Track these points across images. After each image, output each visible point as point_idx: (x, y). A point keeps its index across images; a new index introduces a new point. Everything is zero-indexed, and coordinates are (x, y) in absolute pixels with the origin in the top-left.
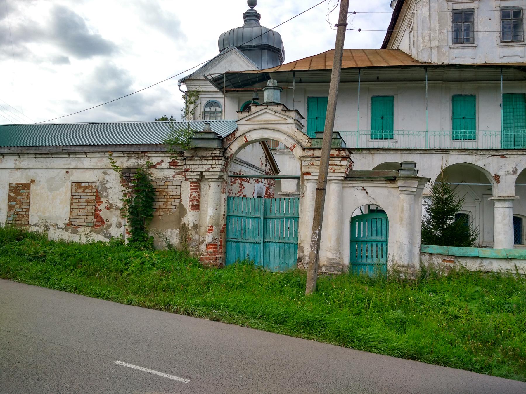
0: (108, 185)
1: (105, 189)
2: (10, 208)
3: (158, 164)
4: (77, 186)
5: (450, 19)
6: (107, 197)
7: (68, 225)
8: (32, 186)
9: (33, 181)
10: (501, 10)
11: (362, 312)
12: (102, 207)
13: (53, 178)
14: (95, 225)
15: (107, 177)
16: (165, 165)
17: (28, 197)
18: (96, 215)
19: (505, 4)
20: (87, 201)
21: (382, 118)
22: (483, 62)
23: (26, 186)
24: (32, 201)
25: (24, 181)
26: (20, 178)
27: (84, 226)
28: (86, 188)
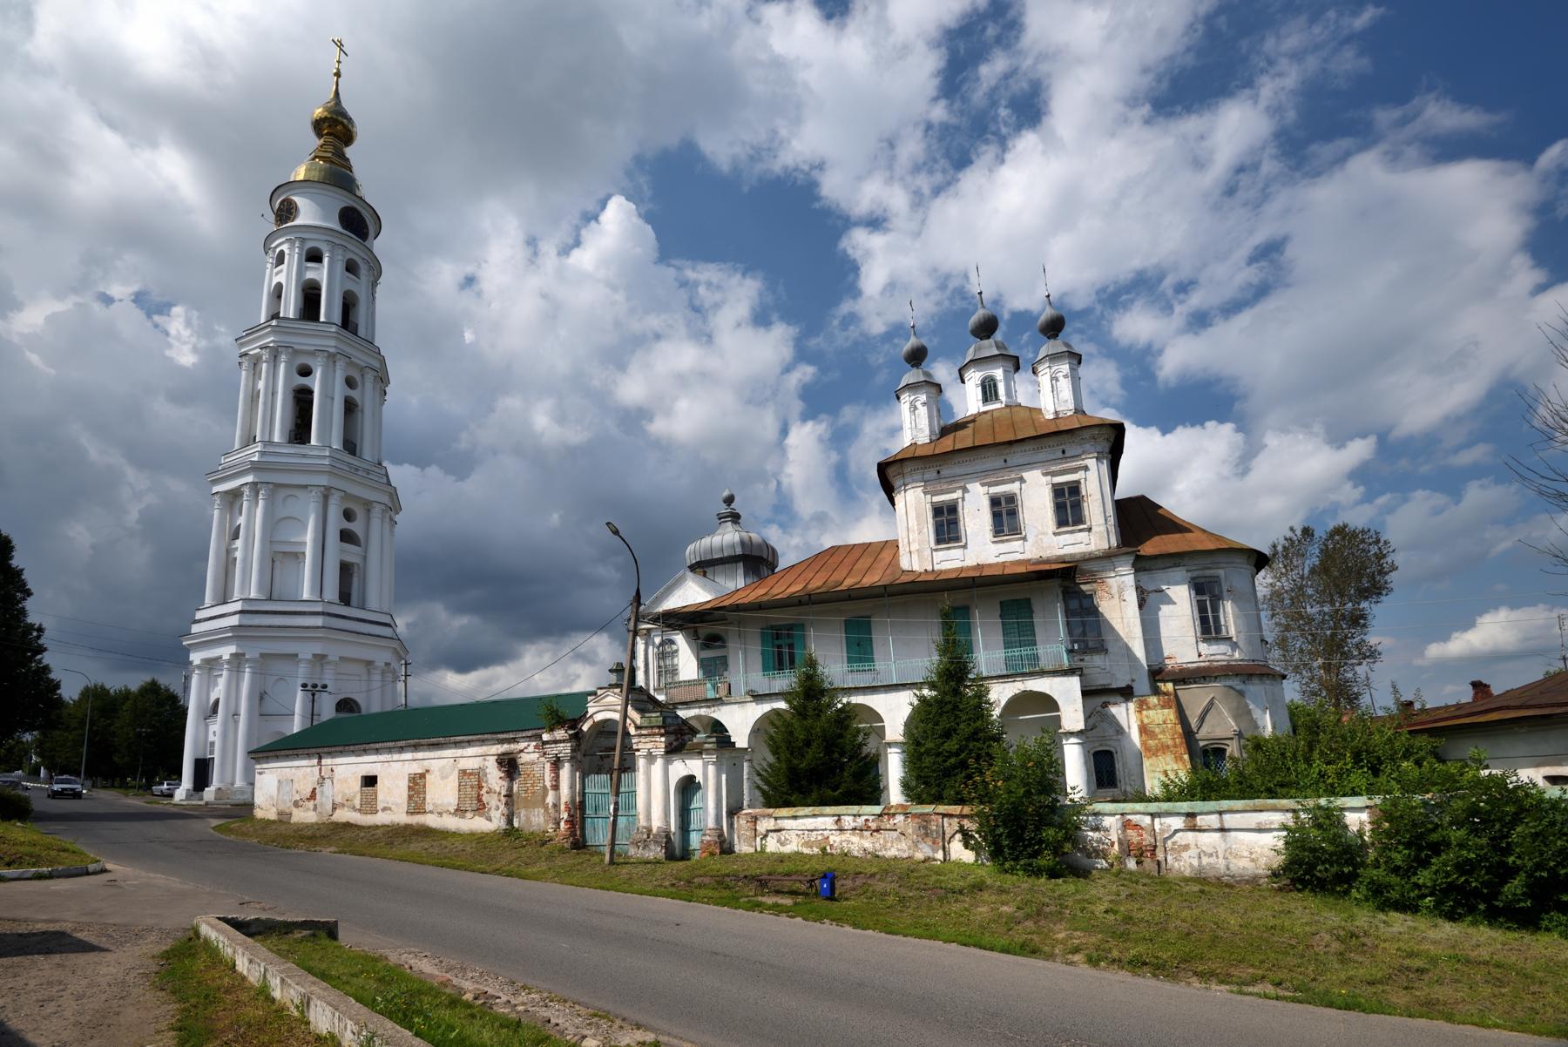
0: (488, 771)
1: (486, 775)
2: (410, 797)
3: (526, 748)
4: (463, 772)
5: (930, 514)
6: (487, 782)
7: (457, 810)
8: (427, 776)
9: (428, 771)
10: (958, 539)
11: (1070, 829)
12: (483, 791)
13: (443, 767)
14: (478, 809)
15: (487, 764)
16: (531, 749)
17: (424, 786)
18: (479, 800)
19: (937, 499)
20: (472, 787)
21: (858, 645)
22: (1037, 557)
23: (422, 776)
24: (427, 790)
25: (420, 771)
26: (416, 768)
27: (510, 789)
28: (471, 774)
